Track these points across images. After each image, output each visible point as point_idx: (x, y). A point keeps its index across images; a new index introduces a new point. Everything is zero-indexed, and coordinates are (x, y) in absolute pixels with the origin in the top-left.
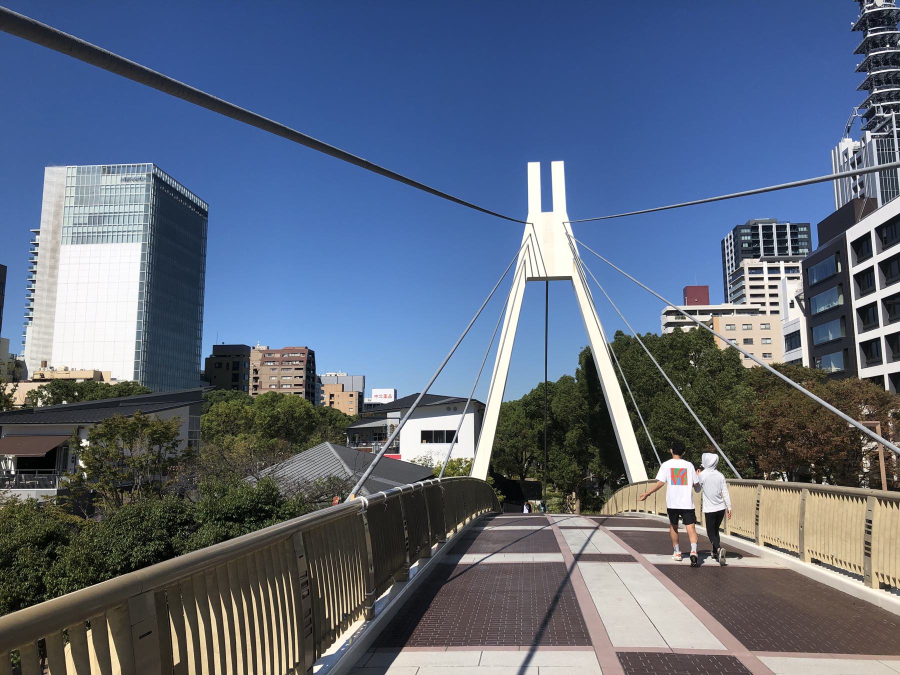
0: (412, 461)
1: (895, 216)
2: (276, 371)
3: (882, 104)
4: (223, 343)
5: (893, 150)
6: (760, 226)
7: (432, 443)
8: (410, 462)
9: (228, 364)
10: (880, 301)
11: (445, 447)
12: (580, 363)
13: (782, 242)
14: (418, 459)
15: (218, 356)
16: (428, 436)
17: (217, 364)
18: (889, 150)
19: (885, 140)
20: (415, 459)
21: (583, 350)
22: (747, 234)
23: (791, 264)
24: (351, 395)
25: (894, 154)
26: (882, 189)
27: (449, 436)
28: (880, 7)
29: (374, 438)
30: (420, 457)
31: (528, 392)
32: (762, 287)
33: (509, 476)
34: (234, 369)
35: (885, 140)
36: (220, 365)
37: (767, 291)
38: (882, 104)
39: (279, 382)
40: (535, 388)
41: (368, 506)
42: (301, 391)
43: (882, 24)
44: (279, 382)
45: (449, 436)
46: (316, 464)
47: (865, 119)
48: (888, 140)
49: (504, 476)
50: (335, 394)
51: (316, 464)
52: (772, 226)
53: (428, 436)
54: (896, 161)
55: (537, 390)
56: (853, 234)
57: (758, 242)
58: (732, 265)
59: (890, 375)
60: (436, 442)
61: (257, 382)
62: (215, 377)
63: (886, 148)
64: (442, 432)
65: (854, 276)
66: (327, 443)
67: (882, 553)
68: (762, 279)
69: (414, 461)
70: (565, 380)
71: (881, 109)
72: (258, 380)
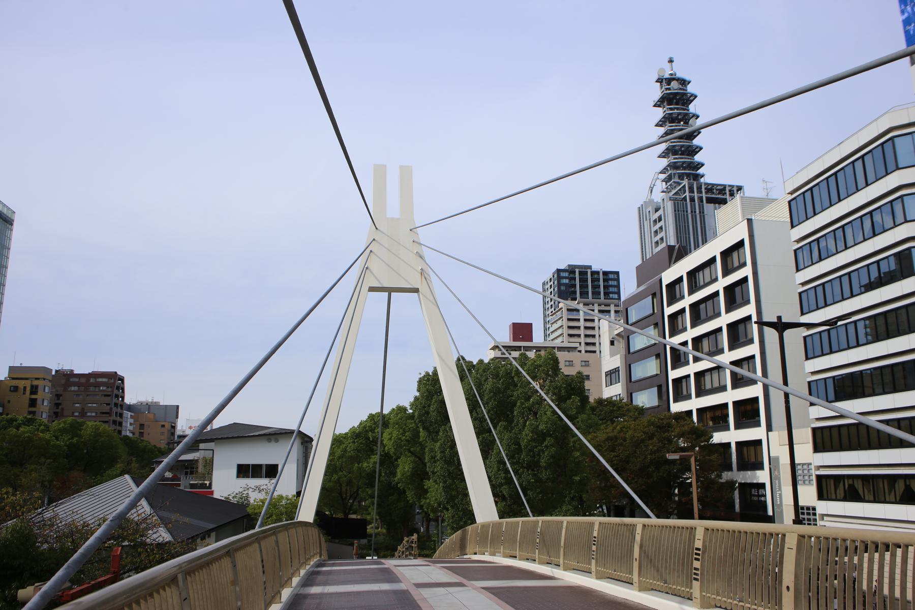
0: (226, 498)
1: (726, 250)
2: (81, 397)
3: (678, 172)
4: (21, 364)
5: (687, 211)
6: (577, 271)
7: (249, 477)
8: (223, 499)
9: (25, 388)
10: (691, 340)
11: (263, 482)
12: (419, 390)
13: (596, 287)
14: (233, 495)
15: (13, 379)
16: (244, 471)
17: (12, 388)
18: (684, 211)
19: (680, 203)
20: (229, 495)
21: (422, 375)
22: (566, 278)
23: (603, 308)
24: (163, 426)
25: (687, 215)
26: (689, 238)
27: (272, 471)
28: (676, 90)
29: (186, 472)
30: (235, 494)
31: (356, 424)
32: (579, 328)
33: (331, 512)
34: (32, 393)
35: (680, 203)
36: (16, 389)
37: (582, 332)
38: (678, 172)
39: (83, 409)
40: (365, 420)
41: (718, 482)
42: (107, 420)
43: (677, 104)
44: (83, 409)
45: (272, 471)
46: (100, 499)
47: (664, 183)
48: (683, 203)
49: (327, 513)
50: (146, 423)
51: (100, 499)
52: (587, 272)
53: (244, 471)
54: (529, 326)
55: (366, 421)
56: (668, 277)
57: (575, 286)
58: (552, 305)
59: (734, 403)
60: (253, 477)
61: (58, 408)
62: (9, 402)
63: (681, 209)
64: (260, 466)
65: (669, 316)
66: (127, 477)
67: (816, 601)
68: (578, 320)
69: (228, 498)
70: (401, 409)
71: (677, 175)
72: (60, 407)
